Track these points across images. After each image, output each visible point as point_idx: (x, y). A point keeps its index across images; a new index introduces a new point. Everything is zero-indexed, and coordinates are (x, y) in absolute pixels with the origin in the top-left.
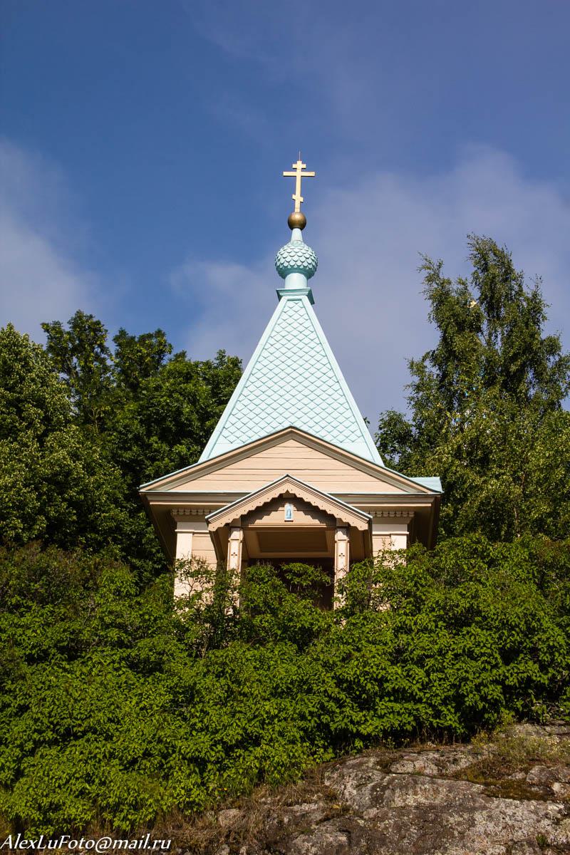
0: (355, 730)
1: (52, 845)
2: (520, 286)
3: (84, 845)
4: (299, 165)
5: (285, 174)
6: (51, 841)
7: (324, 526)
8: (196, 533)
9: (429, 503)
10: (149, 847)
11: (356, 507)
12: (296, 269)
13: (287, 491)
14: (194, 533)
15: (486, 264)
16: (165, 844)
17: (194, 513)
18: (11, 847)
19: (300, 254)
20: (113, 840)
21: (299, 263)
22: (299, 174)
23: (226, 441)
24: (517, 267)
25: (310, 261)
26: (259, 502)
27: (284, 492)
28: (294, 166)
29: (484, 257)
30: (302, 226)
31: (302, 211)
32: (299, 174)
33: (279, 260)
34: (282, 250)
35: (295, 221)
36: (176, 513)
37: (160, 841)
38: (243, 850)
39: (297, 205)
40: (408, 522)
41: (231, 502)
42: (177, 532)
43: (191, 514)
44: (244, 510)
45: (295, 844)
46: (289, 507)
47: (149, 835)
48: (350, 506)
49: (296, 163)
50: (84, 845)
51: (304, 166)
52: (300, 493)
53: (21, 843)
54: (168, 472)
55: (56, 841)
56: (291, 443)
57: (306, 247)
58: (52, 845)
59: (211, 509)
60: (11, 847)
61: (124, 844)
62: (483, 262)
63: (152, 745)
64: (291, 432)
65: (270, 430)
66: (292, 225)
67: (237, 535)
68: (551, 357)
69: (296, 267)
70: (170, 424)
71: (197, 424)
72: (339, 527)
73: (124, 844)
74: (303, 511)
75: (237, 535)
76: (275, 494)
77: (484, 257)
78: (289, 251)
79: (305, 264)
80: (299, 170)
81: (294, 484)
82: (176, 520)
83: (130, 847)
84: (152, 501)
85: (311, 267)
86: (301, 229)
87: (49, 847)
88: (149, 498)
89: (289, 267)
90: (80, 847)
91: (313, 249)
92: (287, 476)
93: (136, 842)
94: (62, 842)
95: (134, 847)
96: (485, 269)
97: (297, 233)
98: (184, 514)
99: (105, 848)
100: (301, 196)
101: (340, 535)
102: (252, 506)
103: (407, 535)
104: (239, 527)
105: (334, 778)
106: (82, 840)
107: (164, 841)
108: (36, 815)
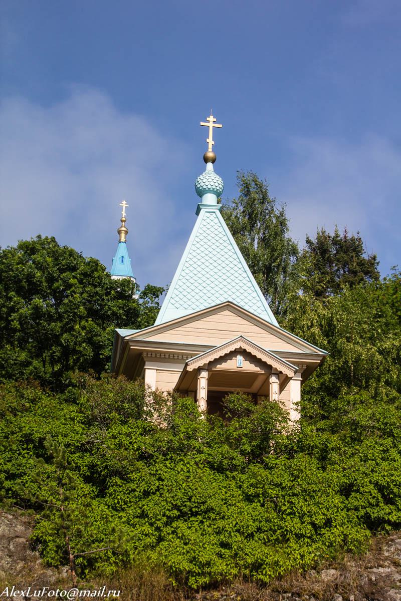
0: (387, 519)
1: (37, 594)
2: (272, 207)
3: (59, 594)
4: (211, 119)
5: (202, 124)
6: (36, 591)
7: (263, 372)
8: (159, 370)
9: (319, 360)
10: (105, 596)
11: (286, 360)
12: (211, 191)
13: (240, 347)
14: (157, 370)
15: (248, 191)
16: (115, 594)
17: (167, 357)
18: (8, 596)
19: (215, 181)
20: (79, 591)
21: (214, 187)
22: (211, 125)
23: (173, 307)
24: (271, 196)
25: (221, 186)
26: (222, 353)
27: (238, 347)
28: (208, 119)
29: (247, 186)
30: (213, 161)
31: (213, 151)
32: (211, 125)
33: (199, 184)
34: (201, 177)
35: (209, 157)
36: (150, 356)
37: (112, 591)
38: (352, 597)
39: (210, 146)
40: (302, 372)
41: (204, 352)
42: (145, 369)
43: (174, 358)
44: (211, 358)
45: (389, 595)
46: (240, 358)
47: (105, 587)
48: (282, 359)
49: (209, 117)
50: (59, 594)
51: (215, 120)
52: (249, 349)
53: (15, 593)
54: (297, 335)
55: (40, 591)
56: (227, 312)
57: (218, 177)
58: (37, 594)
59: (192, 356)
60: (8, 596)
61: (87, 593)
62: (246, 190)
63: (262, 523)
64: (228, 305)
65: (241, 304)
66: (206, 160)
67: (204, 374)
68: (291, 258)
69: (211, 189)
70: (24, 284)
71: (45, 284)
72: (273, 374)
73: (87, 593)
74: (249, 361)
75: (204, 374)
76: (232, 348)
77: (247, 186)
78: (207, 178)
79: (218, 188)
80: (211, 122)
81: (245, 343)
82: (145, 360)
83: (91, 596)
84: (132, 346)
85: (221, 190)
86: (213, 163)
87: (35, 595)
88: (130, 344)
89: (207, 189)
90: (56, 595)
91: (223, 180)
92: (241, 336)
93: (96, 591)
94: (43, 592)
95: (95, 596)
96: (247, 194)
97: (210, 166)
98: (174, 358)
99: (74, 596)
100: (213, 140)
101: (273, 379)
102: (217, 356)
103: (301, 381)
104: (205, 369)
105: (391, 551)
106: (58, 591)
107: (115, 591)
108: (196, 569)
